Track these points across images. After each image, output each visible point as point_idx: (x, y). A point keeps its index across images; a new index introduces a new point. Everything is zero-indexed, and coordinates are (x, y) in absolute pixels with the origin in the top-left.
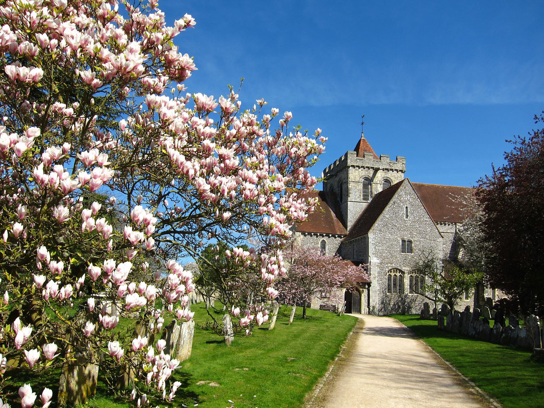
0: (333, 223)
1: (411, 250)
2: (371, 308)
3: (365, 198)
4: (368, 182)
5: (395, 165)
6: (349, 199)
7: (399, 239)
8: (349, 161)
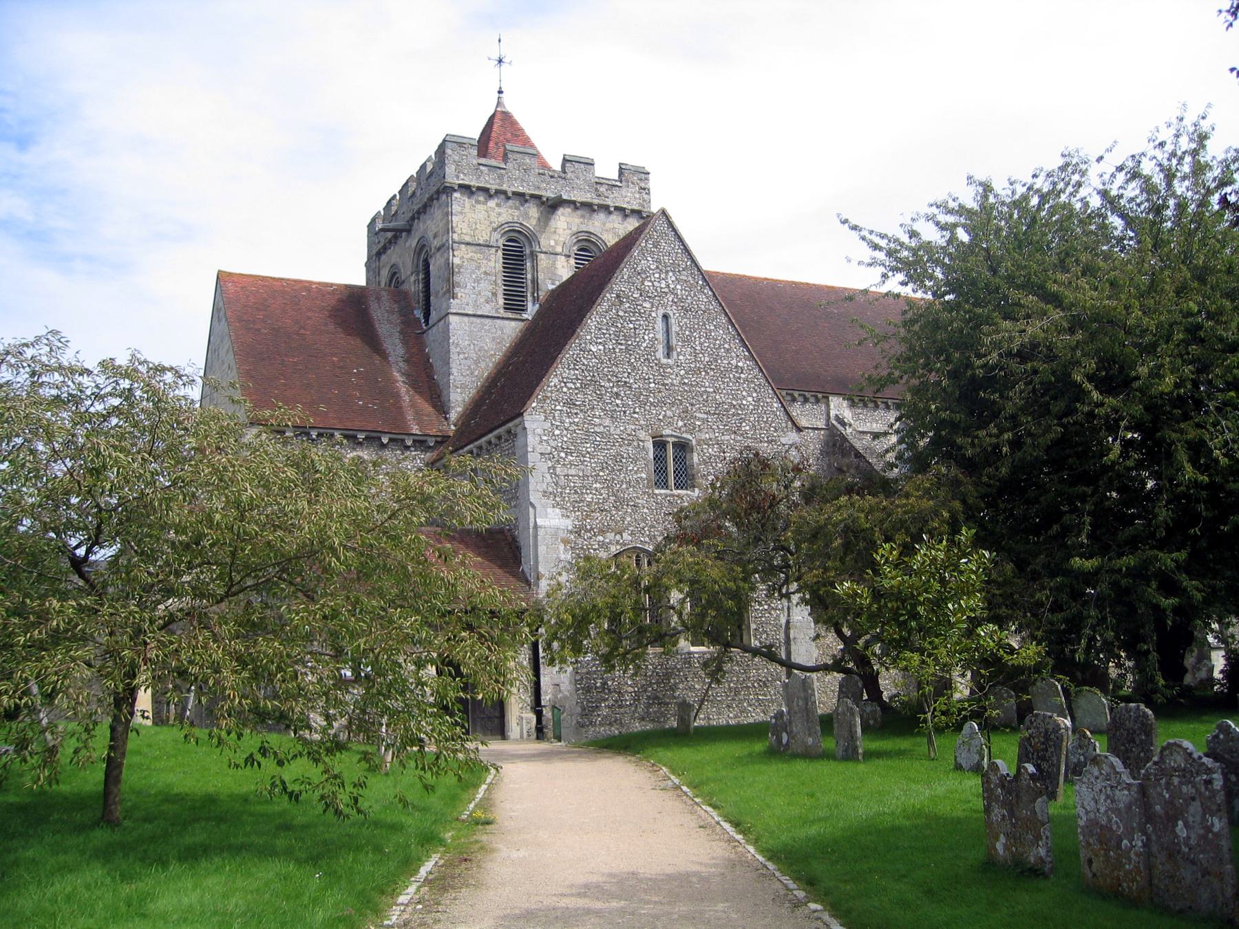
1: (685, 478)
2: (547, 713)
3: (514, 303)
4: (517, 254)
6: (455, 305)
7: (642, 434)
8: (450, 170)
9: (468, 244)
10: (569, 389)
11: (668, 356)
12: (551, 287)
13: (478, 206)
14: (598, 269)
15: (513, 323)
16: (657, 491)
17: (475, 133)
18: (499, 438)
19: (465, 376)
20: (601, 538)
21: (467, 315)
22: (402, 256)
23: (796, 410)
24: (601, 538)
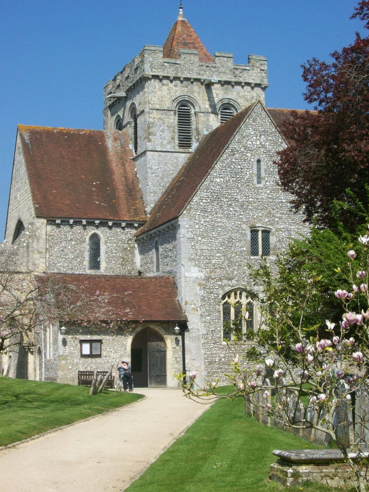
3: (185, 142)
5: (245, 74)
7: (244, 226)
8: (147, 66)
9: (158, 110)
10: (204, 203)
11: (259, 182)
12: (206, 133)
13: (164, 87)
15: (183, 155)
16: (252, 257)
18: (168, 227)
19: (152, 193)
20: (220, 283)
21: (157, 151)
24: (220, 283)
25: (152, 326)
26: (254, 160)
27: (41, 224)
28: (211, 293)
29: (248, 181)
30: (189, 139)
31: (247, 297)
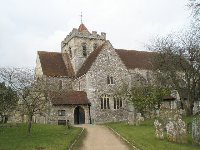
0: (67, 70)
7: (106, 76)
11: (109, 63)
14: (98, 50)
15: (85, 58)
17: (78, 28)
18: (83, 77)
22: (67, 48)
23: (130, 71)
25: (80, 106)
26: (107, 57)
27: (42, 117)
28: (97, 95)
29: (106, 62)
30: (86, 54)
31: (107, 96)
